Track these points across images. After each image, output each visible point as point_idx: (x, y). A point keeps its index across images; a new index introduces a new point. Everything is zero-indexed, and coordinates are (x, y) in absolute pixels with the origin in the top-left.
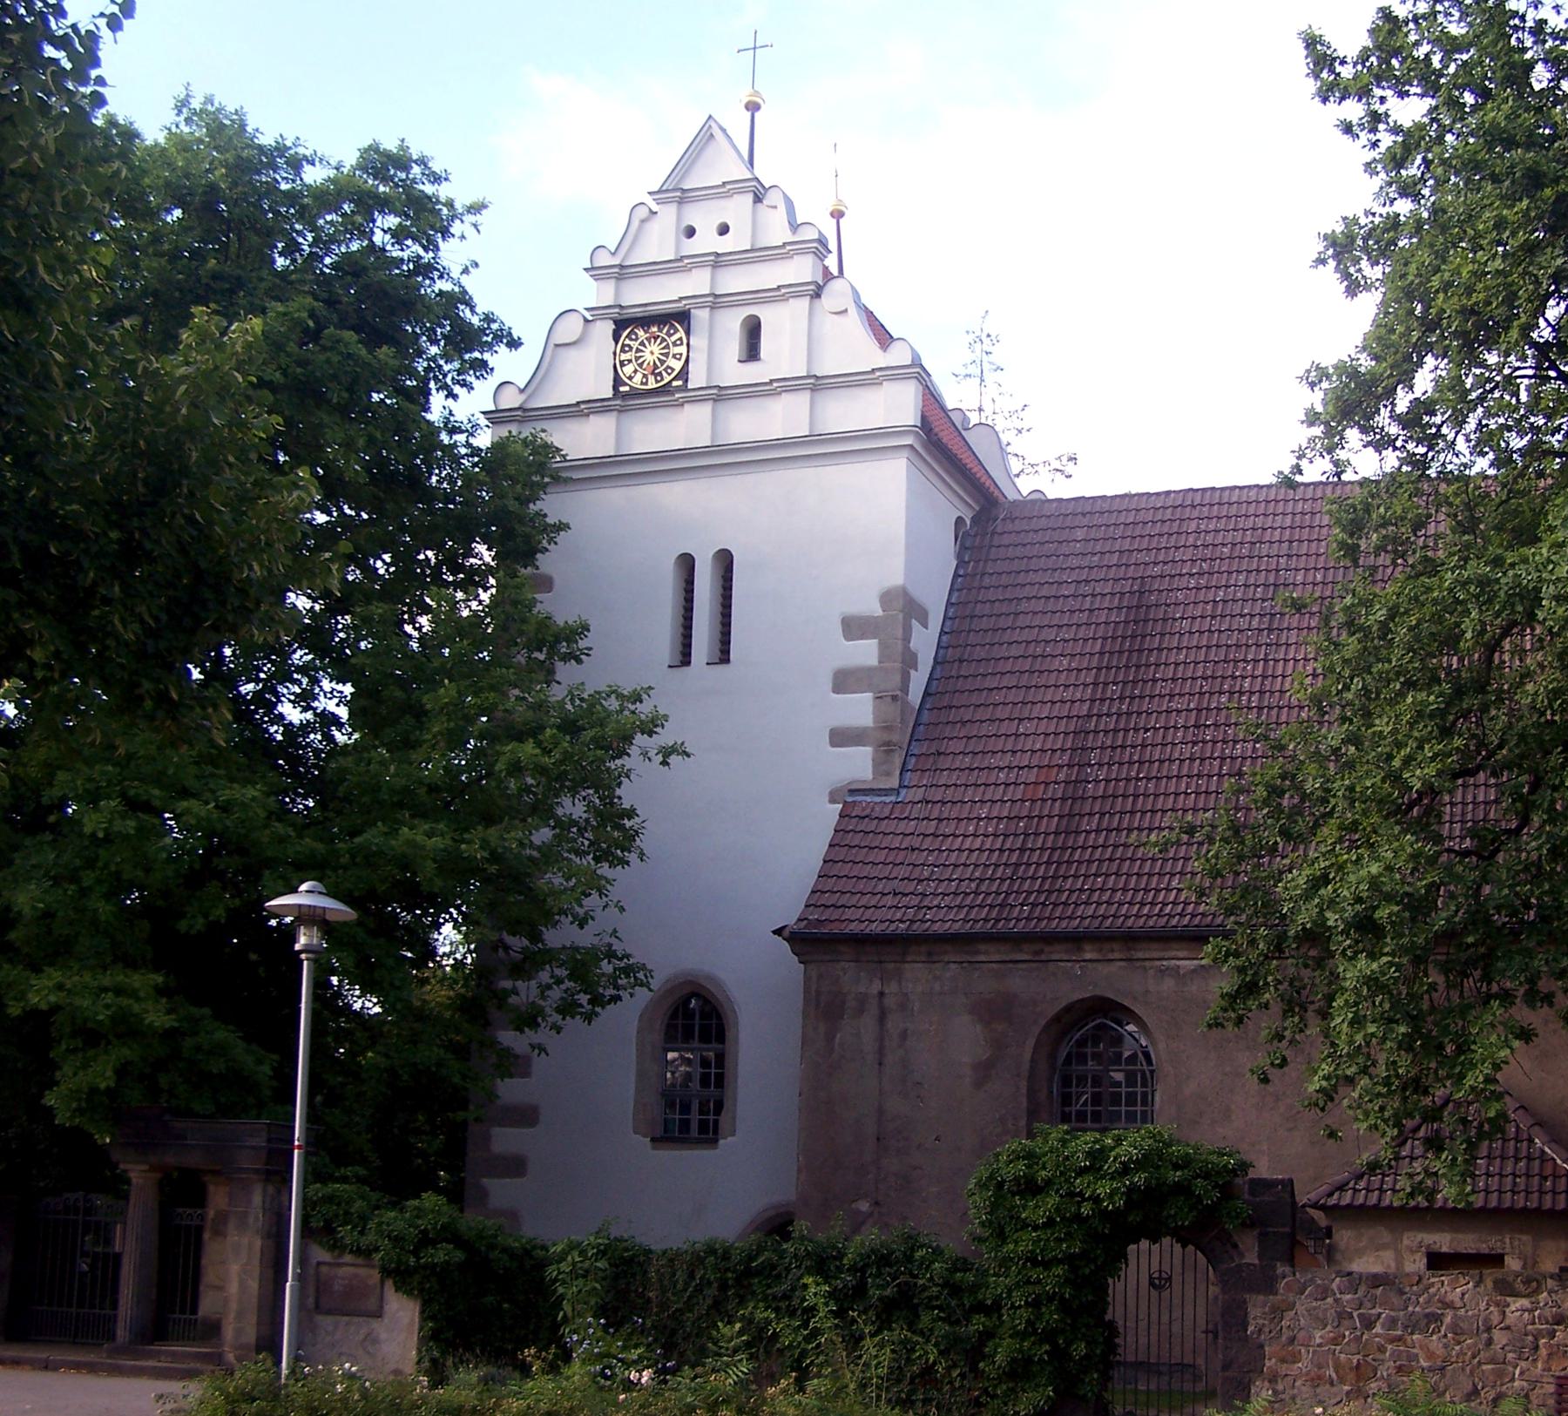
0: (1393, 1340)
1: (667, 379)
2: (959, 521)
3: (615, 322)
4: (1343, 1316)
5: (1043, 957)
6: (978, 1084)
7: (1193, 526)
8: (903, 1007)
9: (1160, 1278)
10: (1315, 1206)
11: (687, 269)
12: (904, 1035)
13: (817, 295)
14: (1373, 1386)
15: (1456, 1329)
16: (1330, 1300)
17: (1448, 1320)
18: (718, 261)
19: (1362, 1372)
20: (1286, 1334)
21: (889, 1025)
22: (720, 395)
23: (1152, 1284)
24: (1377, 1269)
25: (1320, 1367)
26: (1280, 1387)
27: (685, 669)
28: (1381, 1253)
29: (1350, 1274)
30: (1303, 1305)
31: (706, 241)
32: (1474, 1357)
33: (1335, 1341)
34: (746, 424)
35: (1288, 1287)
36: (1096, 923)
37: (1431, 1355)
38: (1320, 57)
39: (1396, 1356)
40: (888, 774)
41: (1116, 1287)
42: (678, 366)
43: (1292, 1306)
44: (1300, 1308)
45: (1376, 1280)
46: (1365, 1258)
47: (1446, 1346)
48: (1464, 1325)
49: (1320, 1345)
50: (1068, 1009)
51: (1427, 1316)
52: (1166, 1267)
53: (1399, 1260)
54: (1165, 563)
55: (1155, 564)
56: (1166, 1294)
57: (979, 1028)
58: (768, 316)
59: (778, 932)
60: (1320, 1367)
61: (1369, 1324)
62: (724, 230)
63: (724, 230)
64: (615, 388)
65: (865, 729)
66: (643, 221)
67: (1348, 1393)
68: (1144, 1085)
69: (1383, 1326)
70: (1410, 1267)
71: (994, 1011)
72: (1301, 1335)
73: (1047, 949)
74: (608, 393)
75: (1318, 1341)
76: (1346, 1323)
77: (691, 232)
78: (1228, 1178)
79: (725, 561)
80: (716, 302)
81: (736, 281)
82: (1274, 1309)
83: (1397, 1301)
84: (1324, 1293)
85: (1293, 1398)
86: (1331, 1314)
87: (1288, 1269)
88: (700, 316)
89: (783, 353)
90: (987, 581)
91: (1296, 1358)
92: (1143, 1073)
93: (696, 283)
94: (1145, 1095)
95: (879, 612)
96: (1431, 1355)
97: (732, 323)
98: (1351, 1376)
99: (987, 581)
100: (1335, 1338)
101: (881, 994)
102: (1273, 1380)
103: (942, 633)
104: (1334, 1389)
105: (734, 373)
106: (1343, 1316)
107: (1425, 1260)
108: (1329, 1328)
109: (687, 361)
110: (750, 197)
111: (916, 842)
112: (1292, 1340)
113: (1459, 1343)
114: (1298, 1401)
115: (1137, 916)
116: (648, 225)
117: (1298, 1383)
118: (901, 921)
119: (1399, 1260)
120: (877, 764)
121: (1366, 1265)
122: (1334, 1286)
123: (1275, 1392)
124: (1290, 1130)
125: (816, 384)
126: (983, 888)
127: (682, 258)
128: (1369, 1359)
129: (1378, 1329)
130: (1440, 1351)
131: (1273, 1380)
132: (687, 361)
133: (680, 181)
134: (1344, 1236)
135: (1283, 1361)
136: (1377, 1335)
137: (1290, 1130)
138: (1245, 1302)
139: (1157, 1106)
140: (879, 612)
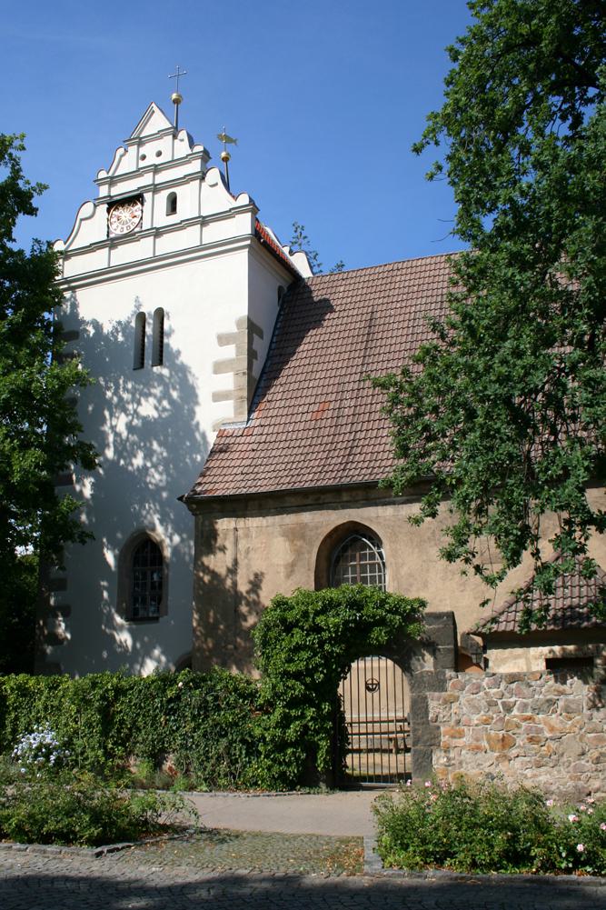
0: (526, 719)
1: (132, 227)
2: (280, 289)
3: (108, 204)
4: (491, 704)
5: (321, 502)
6: (288, 576)
7: (398, 279)
8: (247, 536)
9: (372, 684)
10: (474, 634)
11: (141, 175)
12: (248, 551)
13: (203, 179)
14: (514, 752)
15: (568, 710)
16: (481, 693)
17: (561, 703)
18: (156, 169)
19: (506, 743)
20: (454, 718)
21: (240, 546)
22: (158, 233)
23: (367, 688)
24: (515, 670)
25: (477, 740)
26: (452, 755)
27: (142, 370)
28: (517, 661)
29: (494, 675)
30: (464, 697)
31: (152, 160)
32: (581, 729)
33: (486, 722)
34: (168, 244)
35: (454, 686)
36: (348, 479)
37: (552, 729)
38: (457, 38)
39: (528, 730)
40: (241, 413)
41: (344, 688)
42: (137, 220)
43: (457, 699)
44: (462, 700)
45: (513, 678)
46: (507, 665)
47: (562, 722)
48: (573, 706)
49: (476, 725)
50: (336, 529)
51: (548, 701)
52: (376, 677)
53: (528, 663)
54: (384, 297)
55: (379, 298)
56: (376, 694)
57: (287, 543)
58: (180, 191)
59: (180, 499)
60: (477, 740)
61: (508, 709)
62: (159, 154)
63: (159, 154)
64: (108, 236)
65: (230, 391)
66: (122, 156)
67: (497, 758)
68: (380, 571)
69: (518, 709)
70: (534, 668)
71: (294, 535)
72: (464, 719)
73: (322, 497)
74: (105, 238)
75: (476, 722)
76: (494, 708)
77: (144, 157)
78: (411, 612)
79: (160, 315)
80: (156, 189)
81: (162, 177)
82: (445, 702)
83: (526, 691)
84: (478, 688)
85: (461, 763)
86: (483, 703)
87: (453, 674)
88: (148, 196)
89: (186, 210)
90: (294, 316)
91: (461, 735)
92: (379, 564)
93: (147, 180)
94: (380, 576)
95: (236, 330)
96: (552, 729)
97: (162, 197)
98: (499, 745)
99: (294, 316)
100: (486, 720)
101: (236, 529)
102: (447, 750)
103: (272, 342)
104: (487, 756)
105: (162, 220)
106: (491, 704)
107: (544, 664)
108: (482, 713)
109: (142, 218)
110: (171, 136)
111: (255, 447)
112: (458, 722)
113: (571, 719)
114: (464, 765)
115: (371, 474)
116: (123, 158)
117: (463, 752)
118: (244, 487)
119: (528, 663)
120: (236, 409)
121: (504, 669)
122: (484, 684)
123: (449, 759)
124: (462, 591)
125: (204, 221)
126: (289, 467)
127: (140, 169)
128: (510, 733)
129: (515, 712)
130: (558, 726)
131: (447, 750)
132: (142, 218)
133: (140, 133)
134: (493, 654)
135: (453, 737)
136: (515, 716)
137: (462, 591)
138: (426, 698)
139: (387, 584)
140: (236, 330)
